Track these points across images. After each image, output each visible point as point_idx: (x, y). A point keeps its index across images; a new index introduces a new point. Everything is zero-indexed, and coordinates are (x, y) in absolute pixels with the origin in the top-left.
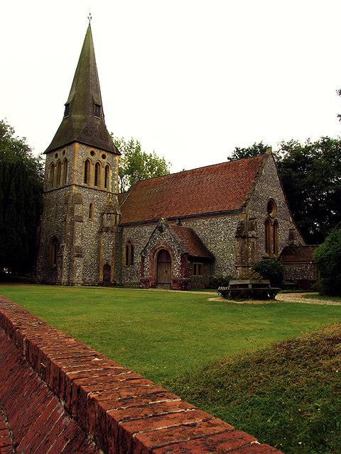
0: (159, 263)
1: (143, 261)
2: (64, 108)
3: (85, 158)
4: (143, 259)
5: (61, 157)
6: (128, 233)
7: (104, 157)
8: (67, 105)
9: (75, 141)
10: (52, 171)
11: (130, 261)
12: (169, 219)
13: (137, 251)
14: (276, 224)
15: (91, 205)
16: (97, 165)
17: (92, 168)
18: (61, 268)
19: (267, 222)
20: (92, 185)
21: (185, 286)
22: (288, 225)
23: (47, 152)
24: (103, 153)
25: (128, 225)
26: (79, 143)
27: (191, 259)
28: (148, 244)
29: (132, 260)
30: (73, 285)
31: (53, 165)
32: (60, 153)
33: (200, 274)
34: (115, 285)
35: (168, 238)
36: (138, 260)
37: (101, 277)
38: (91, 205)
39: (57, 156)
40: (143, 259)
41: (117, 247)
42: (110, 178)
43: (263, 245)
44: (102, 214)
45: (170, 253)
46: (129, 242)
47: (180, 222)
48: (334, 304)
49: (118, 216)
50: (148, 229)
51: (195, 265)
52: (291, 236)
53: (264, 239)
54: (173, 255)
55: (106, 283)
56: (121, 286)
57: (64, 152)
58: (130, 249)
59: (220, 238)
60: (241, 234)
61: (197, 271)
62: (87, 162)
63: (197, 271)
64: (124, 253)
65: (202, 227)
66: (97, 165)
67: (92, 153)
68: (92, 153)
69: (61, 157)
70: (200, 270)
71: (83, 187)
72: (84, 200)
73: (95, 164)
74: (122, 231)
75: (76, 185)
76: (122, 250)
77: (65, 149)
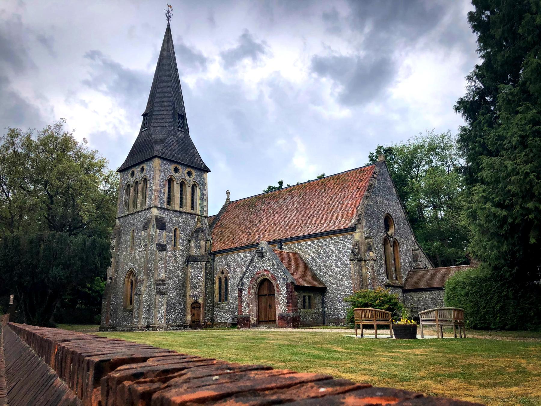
0: (259, 295)
1: (240, 296)
2: (141, 119)
3: (167, 176)
4: (240, 291)
5: (139, 176)
6: (221, 262)
7: (189, 174)
8: (145, 115)
9: (156, 156)
10: (128, 193)
11: (224, 297)
12: (270, 243)
13: (233, 283)
14: (395, 244)
15: (176, 230)
16: (182, 184)
17: (176, 188)
18: (139, 309)
19: (385, 242)
20: (177, 208)
21: (296, 322)
22: (410, 245)
23: (121, 170)
24: (187, 170)
25: (221, 252)
26: (161, 158)
27: (298, 288)
28: (245, 273)
29: (226, 294)
30: (154, 329)
31: (129, 185)
32: (137, 170)
33: (310, 308)
34: (205, 326)
35: (266, 266)
36: (233, 293)
37: (189, 317)
38: (176, 230)
39: (133, 173)
40: (240, 291)
41: (209, 279)
42: (198, 198)
43: (383, 269)
44: (189, 241)
45: (274, 283)
46: (222, 273)
47: (281, 245)
48: (481, 337)
49: (208, 244)
50: (243, 257)
51: (304, 297)
52: (415, 258)
53: (383, 262)
54: (277, 285)
55: (195, 325)
56: (210, 327)
57: (142, 170)
58: (223, 281)
59: (336, 266)
60: (357, 257)
61: (307, 304)
62: (170, 181)
63: (307, 304)
64: (217, 286)
65: (308, 251)
66: (182, 184)
67: (189, 174)
68: (176, 170)
69: (139, 176)
70: (310, 303)
71: (166, 209)
72: (168, 225)
73: (179, 182)
74: (213, 260)
75: (157, 208)
76: (213, 283)
77: (144, 166)
